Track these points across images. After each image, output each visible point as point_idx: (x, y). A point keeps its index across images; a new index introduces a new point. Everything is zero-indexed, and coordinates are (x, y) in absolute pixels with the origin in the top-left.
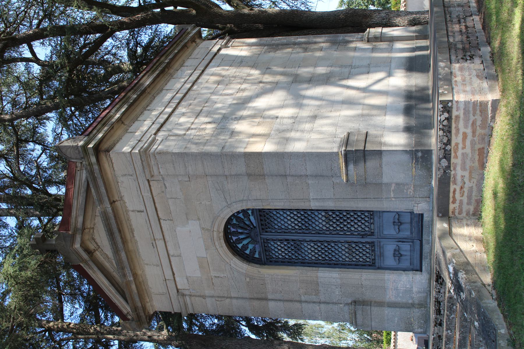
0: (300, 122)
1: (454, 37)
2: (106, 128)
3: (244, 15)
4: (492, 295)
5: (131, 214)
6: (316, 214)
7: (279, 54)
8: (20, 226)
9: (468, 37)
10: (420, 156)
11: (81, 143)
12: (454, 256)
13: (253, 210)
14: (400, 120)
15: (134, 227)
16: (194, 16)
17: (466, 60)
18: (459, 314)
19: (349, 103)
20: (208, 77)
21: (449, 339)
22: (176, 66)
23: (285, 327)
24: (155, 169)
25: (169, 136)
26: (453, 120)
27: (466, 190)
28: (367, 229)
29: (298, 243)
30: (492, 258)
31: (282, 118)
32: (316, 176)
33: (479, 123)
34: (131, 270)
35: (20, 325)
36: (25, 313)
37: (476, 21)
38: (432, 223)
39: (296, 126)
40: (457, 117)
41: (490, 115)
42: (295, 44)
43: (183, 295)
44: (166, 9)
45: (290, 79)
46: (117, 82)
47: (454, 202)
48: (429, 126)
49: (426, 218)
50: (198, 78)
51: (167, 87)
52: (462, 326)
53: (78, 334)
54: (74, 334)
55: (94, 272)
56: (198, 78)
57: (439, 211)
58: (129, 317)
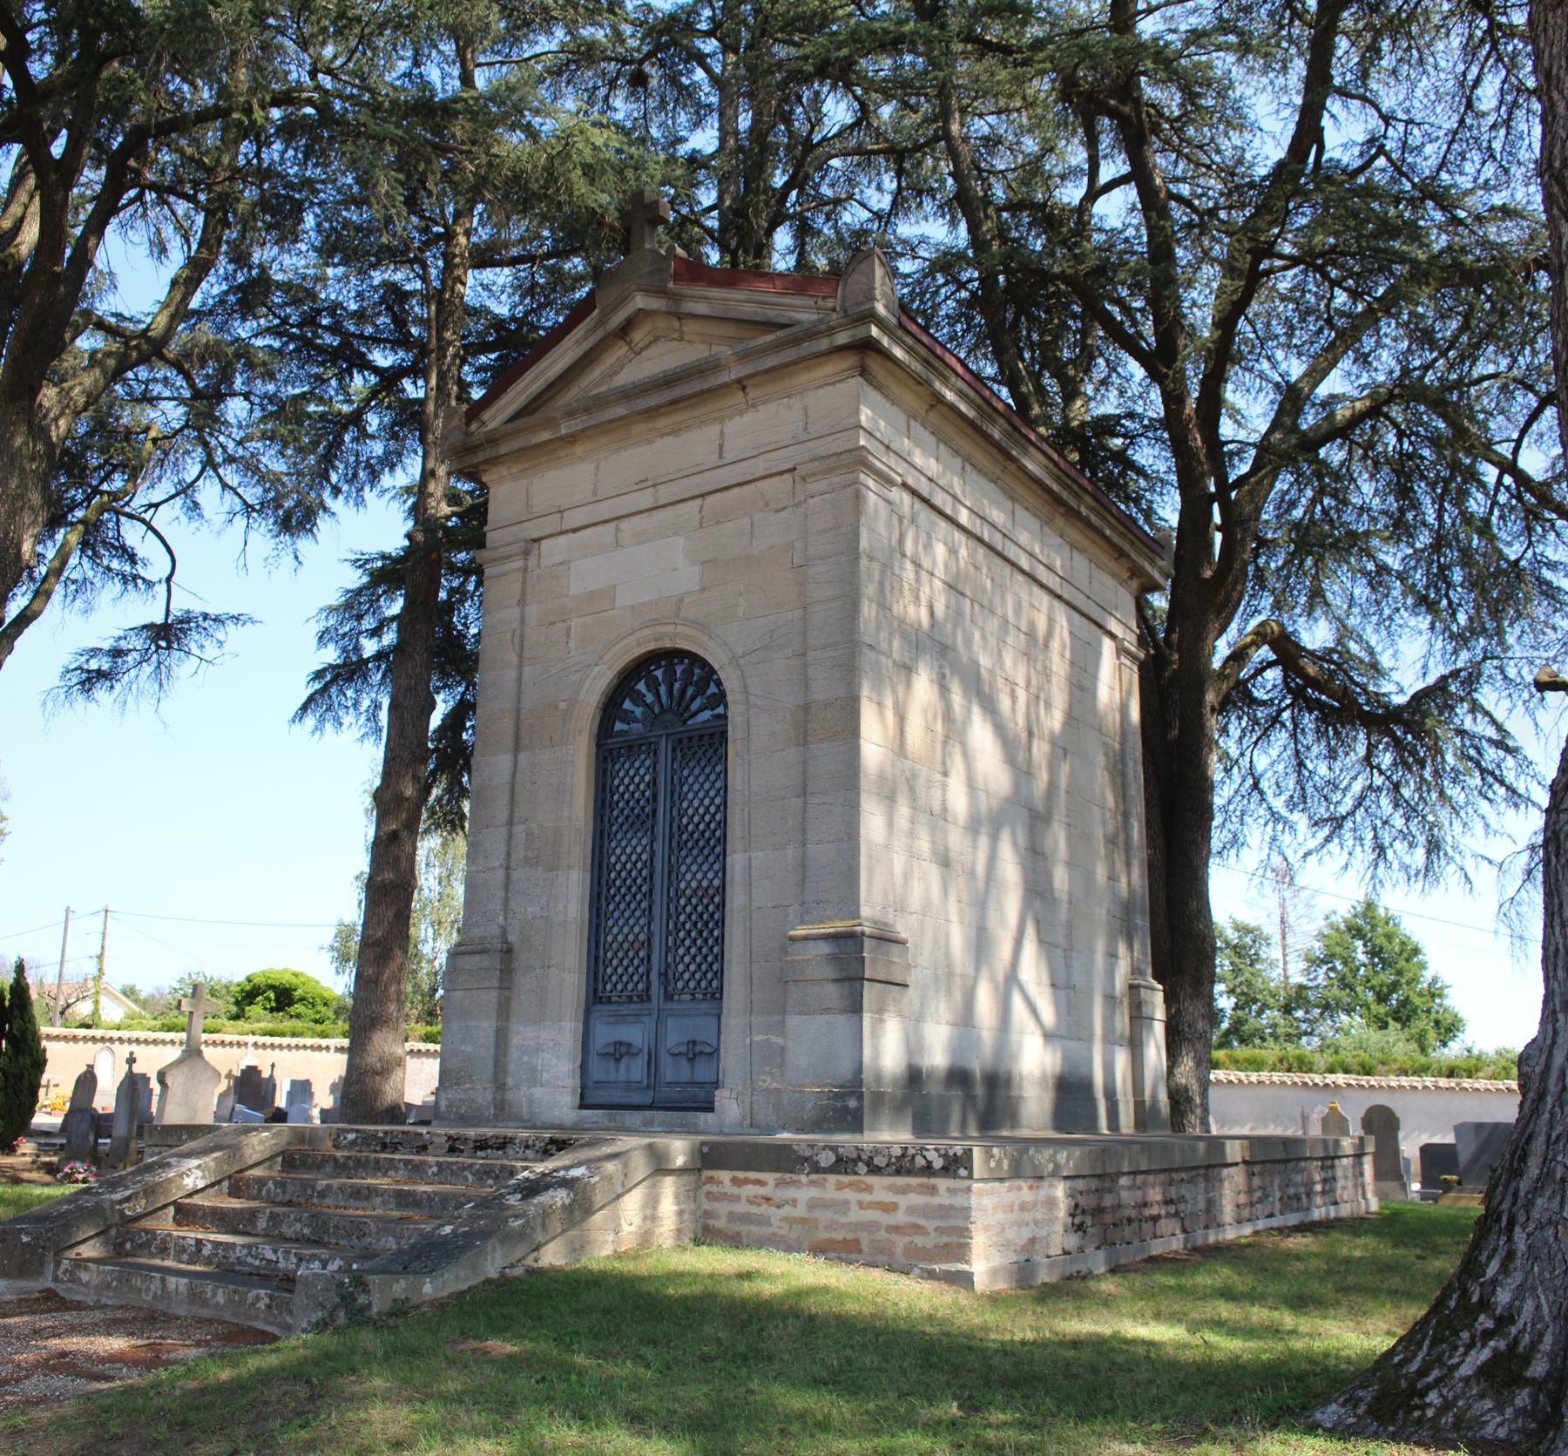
0: (933, 829)
1: (1132, 1187)
2: (916, 366)
3: (1202, 694)
4: (512, 1266)
5: (716, 428)
6: (717, 866)
7: (1102, 778)
8: (695, 161)
9: (1130, 1220)
10: (849, 1103)
11: (880, 309)
12: (609, 1178)
13: (725, 717)
14: (937, 1058)
15: (686, 436)
16: (1198, 574)
17: (1073, 1215)
18: (472, 1192)
19: (981, 943)
20: (1044, 609)
21: (417, 1170)
22: (1074, 533)
23: (457, 791)
24: (820, 485)
25: (901, 519)
26: (925, 1180)
27: (763, 1209)
28: (680, 984)
29: (649, 824)
30: (595, 1266)
31: (944, 786)
32: (804, 866)
33: (919, 1240)
34: (583, 431)
35: (455, 167)
36: (484, 179)
37: (1171, 1241)
38: (687, 1130)
39: (923, 819)
40: (933, 1190)
41: (936, 1267)
42: (1126, 815)
43: (526, 553)
44: (1216, 507)
45: (1040, 806)
46: (1041, 391)
47: (779, 1184)
48: (922, 1125)
49: (703, 1118)
50: (1042, 586)
51: (1019, 511)
52: (445, 1198)
53: (440, 304)
54: (441, 292)
55: (578, 342)
56: (1042, 586)
57: (714, 1146)
58: (474, 426)
